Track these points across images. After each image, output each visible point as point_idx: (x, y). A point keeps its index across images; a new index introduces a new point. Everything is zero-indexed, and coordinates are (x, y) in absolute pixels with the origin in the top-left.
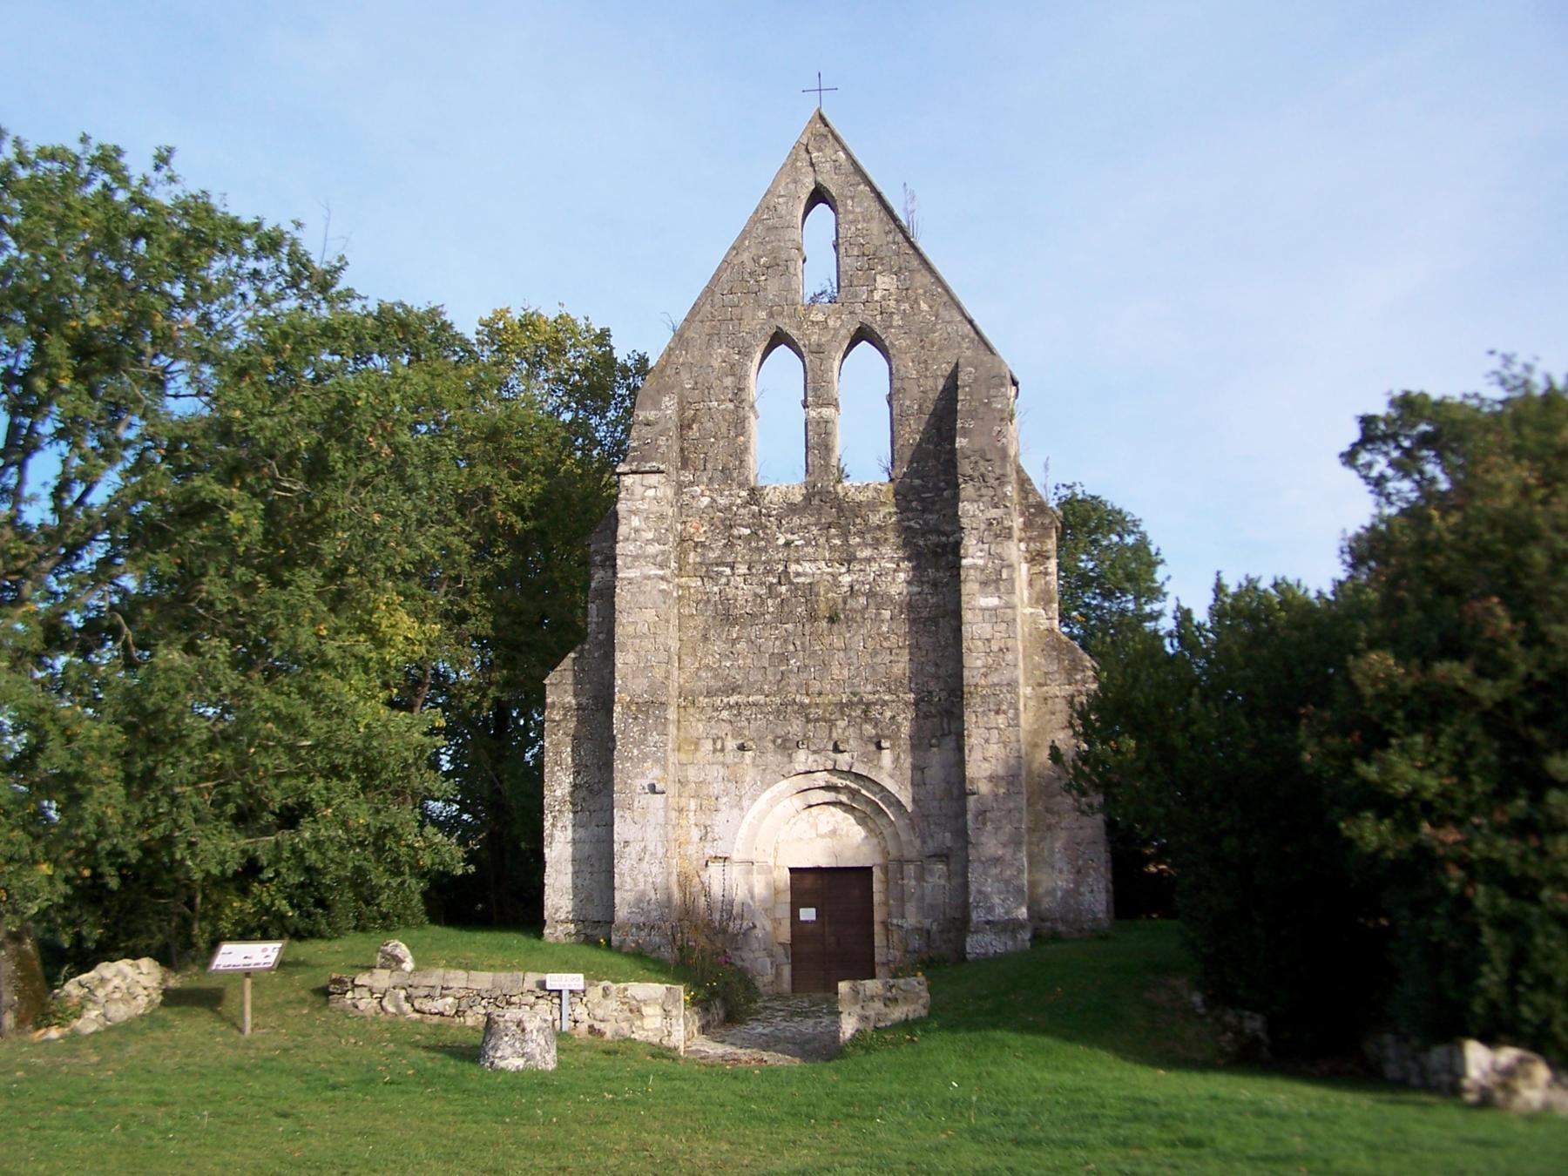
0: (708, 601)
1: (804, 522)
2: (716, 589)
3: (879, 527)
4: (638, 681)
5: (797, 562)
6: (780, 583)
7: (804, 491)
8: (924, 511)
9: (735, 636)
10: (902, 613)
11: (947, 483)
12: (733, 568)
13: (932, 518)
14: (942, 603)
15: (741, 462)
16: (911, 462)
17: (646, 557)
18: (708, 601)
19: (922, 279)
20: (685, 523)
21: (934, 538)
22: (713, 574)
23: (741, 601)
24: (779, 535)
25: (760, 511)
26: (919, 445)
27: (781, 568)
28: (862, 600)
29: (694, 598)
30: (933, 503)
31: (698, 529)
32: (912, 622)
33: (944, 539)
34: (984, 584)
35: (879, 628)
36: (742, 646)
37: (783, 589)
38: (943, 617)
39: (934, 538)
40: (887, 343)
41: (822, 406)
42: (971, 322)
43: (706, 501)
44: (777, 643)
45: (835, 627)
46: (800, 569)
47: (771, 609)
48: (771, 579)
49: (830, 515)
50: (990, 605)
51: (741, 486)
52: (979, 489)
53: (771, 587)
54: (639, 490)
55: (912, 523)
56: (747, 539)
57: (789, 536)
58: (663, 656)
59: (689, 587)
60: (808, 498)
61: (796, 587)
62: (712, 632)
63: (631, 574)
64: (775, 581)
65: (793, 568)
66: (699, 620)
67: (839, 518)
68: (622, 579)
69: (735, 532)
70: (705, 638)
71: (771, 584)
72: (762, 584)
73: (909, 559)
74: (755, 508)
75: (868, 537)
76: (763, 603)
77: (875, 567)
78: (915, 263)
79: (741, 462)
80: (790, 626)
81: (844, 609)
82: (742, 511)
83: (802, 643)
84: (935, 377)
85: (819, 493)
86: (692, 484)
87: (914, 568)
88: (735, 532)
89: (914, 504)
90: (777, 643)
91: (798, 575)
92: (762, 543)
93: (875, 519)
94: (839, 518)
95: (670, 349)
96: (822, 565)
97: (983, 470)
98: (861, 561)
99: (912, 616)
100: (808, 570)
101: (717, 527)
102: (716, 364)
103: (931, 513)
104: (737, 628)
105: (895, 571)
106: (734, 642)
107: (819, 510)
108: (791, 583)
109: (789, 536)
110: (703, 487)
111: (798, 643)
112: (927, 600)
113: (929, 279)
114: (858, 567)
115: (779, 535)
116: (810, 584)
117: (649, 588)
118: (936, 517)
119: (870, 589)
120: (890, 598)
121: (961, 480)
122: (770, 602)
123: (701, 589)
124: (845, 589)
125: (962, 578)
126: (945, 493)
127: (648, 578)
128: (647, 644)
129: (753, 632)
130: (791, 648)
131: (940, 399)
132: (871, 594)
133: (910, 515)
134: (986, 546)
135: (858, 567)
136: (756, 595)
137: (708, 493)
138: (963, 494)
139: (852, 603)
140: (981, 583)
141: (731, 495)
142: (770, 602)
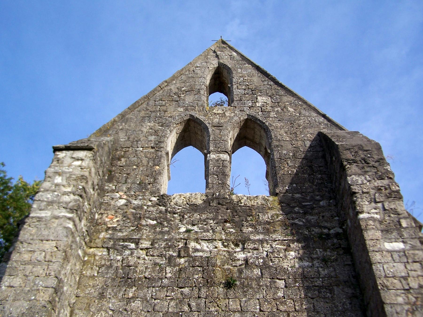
0: (111, 266)
1: (204, 216)
2: (119, 258)
3: (269, 223)
4: (17, 303)
5: (197, 240)
6: (179, 256)
7: (204, 198)
8: (305, 213)
9: (131, 295)
10: (296, 282)
11: (321, 196)
12: (137, 244)
13: (313, 218)
14: (333, 274)
15: (155, 179)
16: (291, 184)
17: (59, 203)
18: (111, 266)
19: (287, 99)
20: (102, 214)
21: (317, 230)
22: (118, 247)
23: (140, 268)
24: (180, 225)
25: (166, 210)
26: (296, 174)
27: (181, 245)
28: (257, 272)
29: (98, 263)
30: (313, 208)
31: (112, 219)
32: (307, 289)
33: (326, 231)
34: (386, 231)
35: (275, 293)
36: (137, 304)
37: (182, 260)
38: (338, 285)
39: (317, 230)
40: (267, 124)
41: (220, 152)
42: (324, 116)
43: (122, 202)
44: (172, 303)
45: (231, 292)
46: (198, 247)
47: (169, 275)
48: (171, 253)
49: (225, 214)
50: (397, 249)
51: (153, 193)
52: (363, 168)
53: (170, 259)
54: (68, 161)
55: (296, 221)
56: (153, 227)
57: (190, 227)
58: (53, 282)
59: (95, 255)
60: (207, 202)
61: (195, 259)
62: (109, 290)
63: (43, 214)
64: (175, 254)
65: (192, 244)
66: (99, 282)
67: (234, 216)
68: (33, 217)
69: (144, 223)
70: (102, 296)
71: (171, 256)
72: (161, 256)
73: (298, 241)
74: (163, 208)
75: (260, 228)
76: (162, 270)
77: (267, 248)
78: (282, 92)
79: (155, 179)
80: (186, 290)
81: (240, 278)
82: (151, 209)
83: (198, 305)
84: (304, 141)
85: (217, 198)
86: (113, 191)
87: (303, 248)
88: (144, 223)
89: (296, 209)
90: (172, 303)
91: (197, 250)
92: (167, 229)
93: (265, 217)
94: (234, 216)
95: (115, 121)
96: (219, 244)
97: (362, 156)
98: (254, 242)
99: (306, 284)
100: (205, 248)
101: (128, 218)
102: (145, 130)
103: (311, 214)
104: (134, 289)
105: (285, 250)
106: (129, 300)
107: (217, 211)
108: (189, 256)
109: (190, 227)
110: (121, 193)
111: (193, 304)
112: (318, 272)
113: (292, 99)
114: (252, 246)
115: (180, 225)
116: (208, 257)
117: (55, 225)
118: (316, 217)
119: (264, 263)
120: (285, 271)
121: (345, 163)
122: (168, 269)
123: (106, 257)
124: (240, 262)
125: (363, 227)
126: (321, 203)
127: (57, 218)
128: (39, 270)
129: (149, 293)
130: (186, 308)
131: (308, 151)
132: (264, 267)
133: (294, 216)
134: (380, 205)
135: (252, 246)
136: (156, 264)
137: (125, 197)
138: (349, 172)
139: (247, 273)
140: (382, 231)
141: (144, 199)
142: (168, 269)
